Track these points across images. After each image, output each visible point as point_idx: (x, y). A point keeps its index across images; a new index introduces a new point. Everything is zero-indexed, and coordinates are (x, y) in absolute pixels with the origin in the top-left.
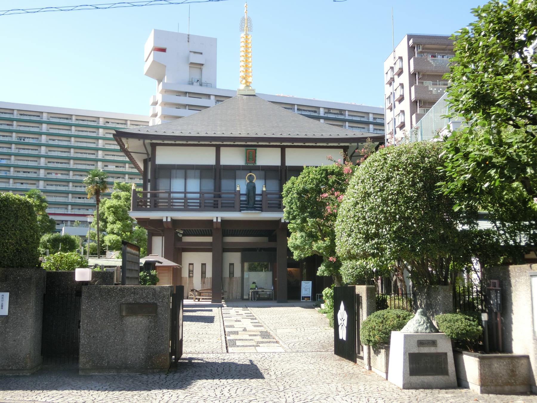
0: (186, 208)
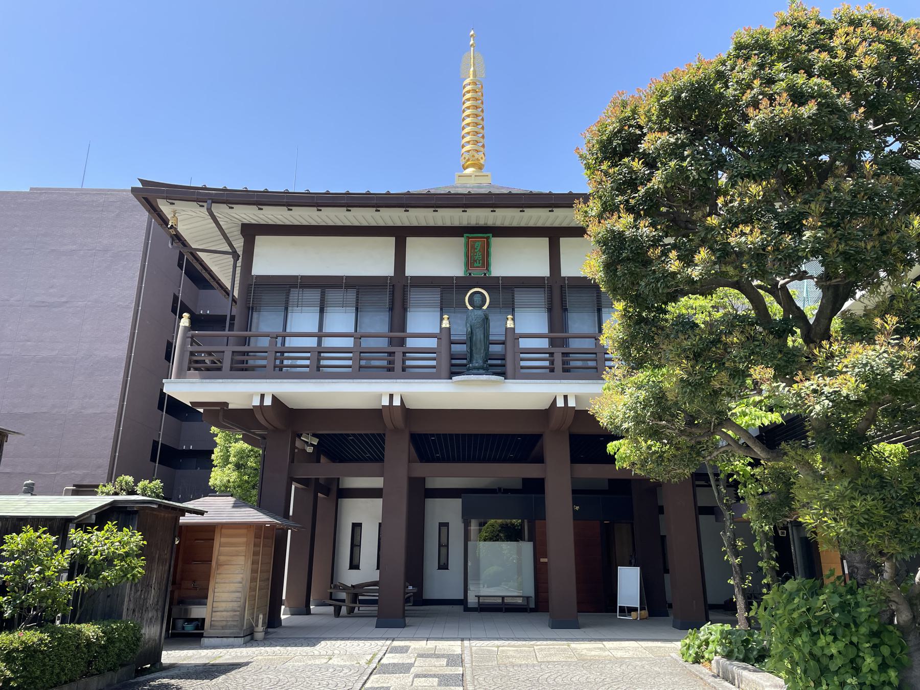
0: (317, 371)
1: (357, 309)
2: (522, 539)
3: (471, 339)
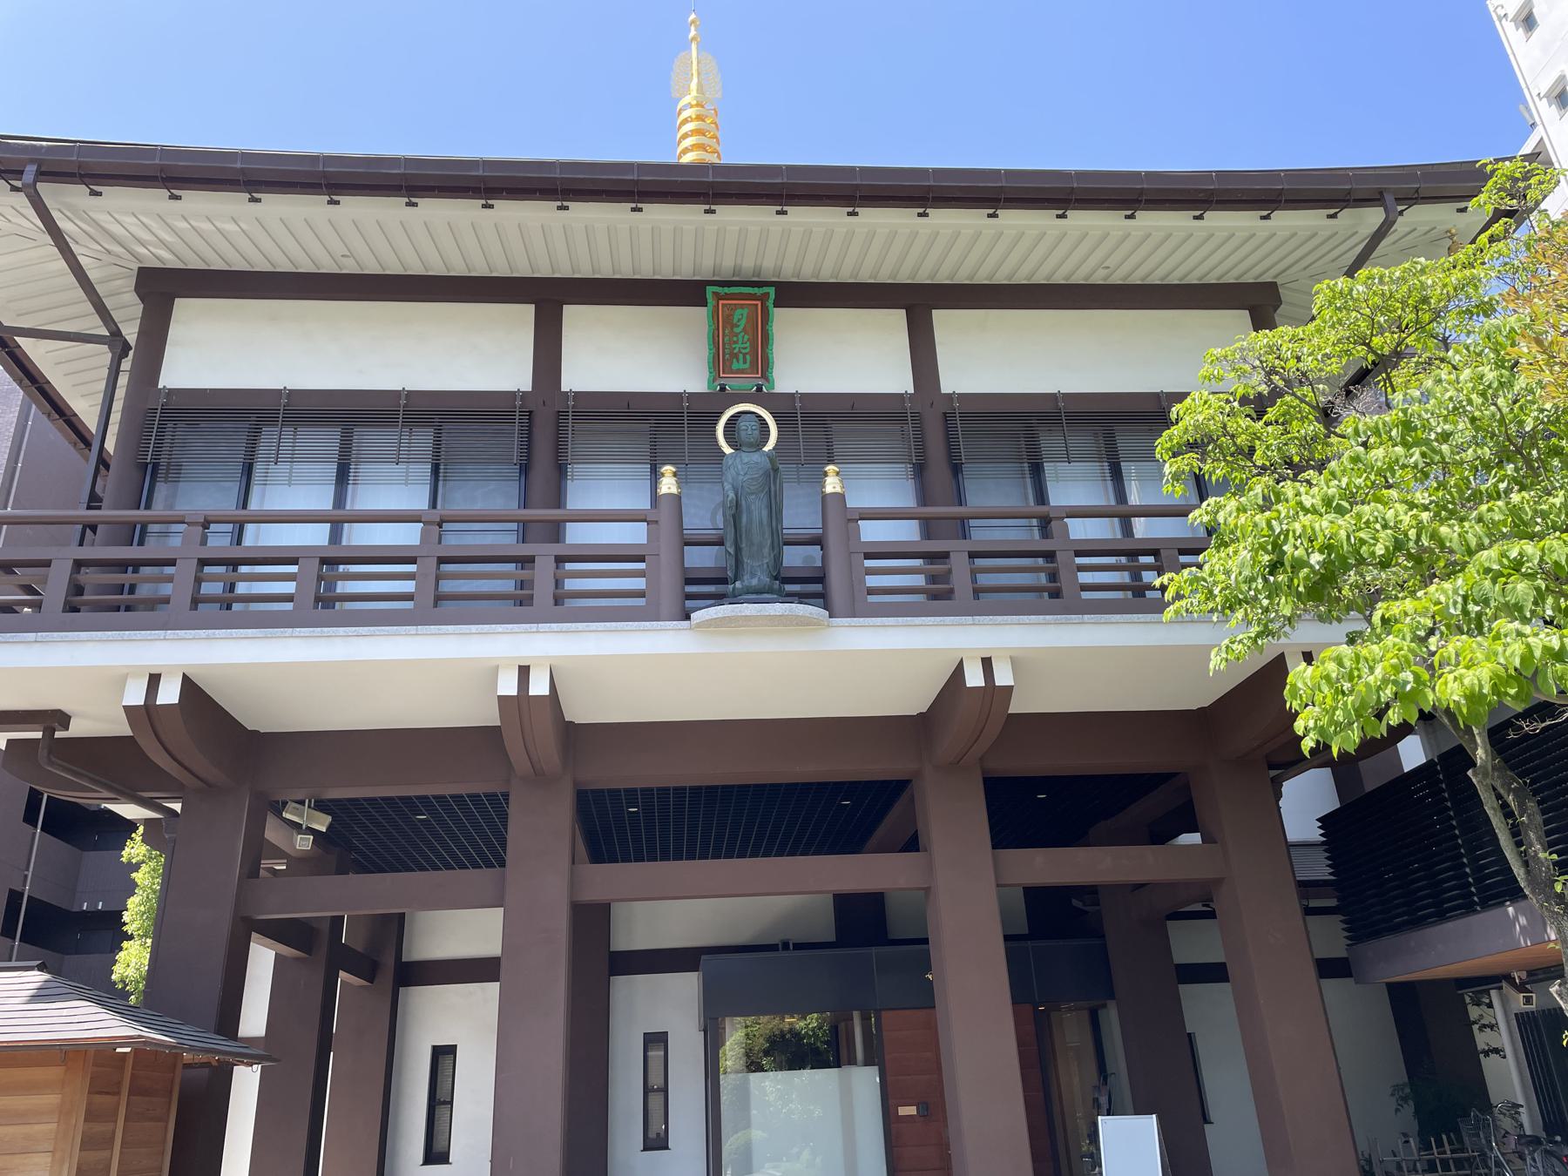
1: (436, 470)
2: (852, 1061)
3: (736, 518)
